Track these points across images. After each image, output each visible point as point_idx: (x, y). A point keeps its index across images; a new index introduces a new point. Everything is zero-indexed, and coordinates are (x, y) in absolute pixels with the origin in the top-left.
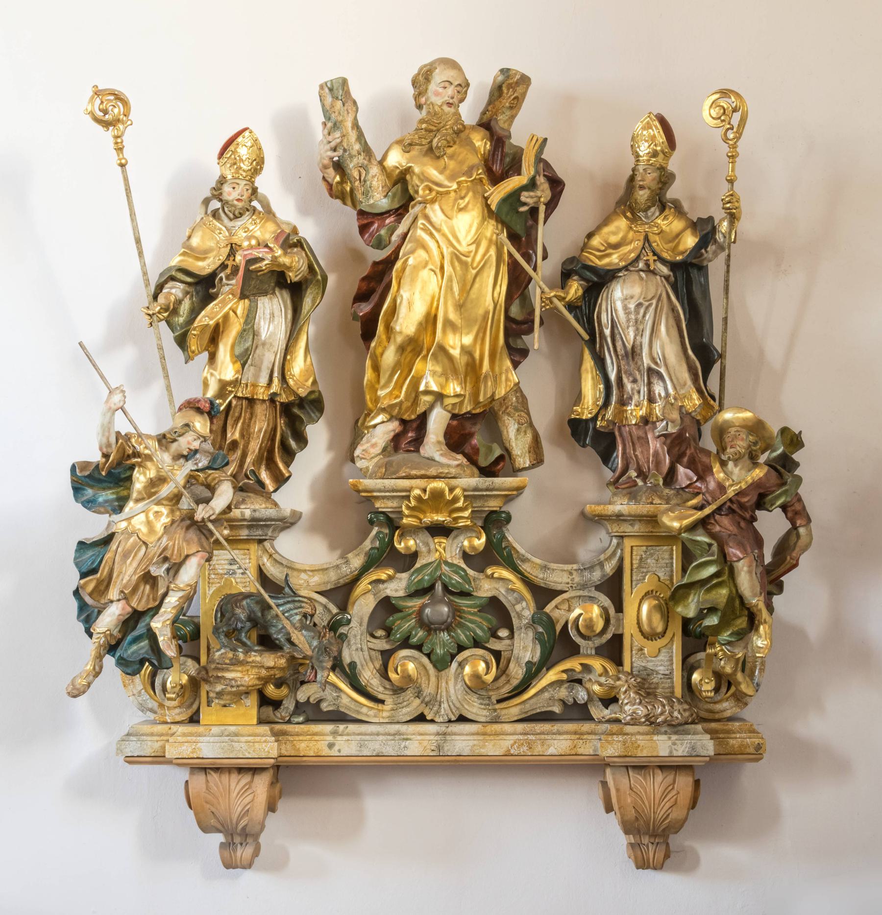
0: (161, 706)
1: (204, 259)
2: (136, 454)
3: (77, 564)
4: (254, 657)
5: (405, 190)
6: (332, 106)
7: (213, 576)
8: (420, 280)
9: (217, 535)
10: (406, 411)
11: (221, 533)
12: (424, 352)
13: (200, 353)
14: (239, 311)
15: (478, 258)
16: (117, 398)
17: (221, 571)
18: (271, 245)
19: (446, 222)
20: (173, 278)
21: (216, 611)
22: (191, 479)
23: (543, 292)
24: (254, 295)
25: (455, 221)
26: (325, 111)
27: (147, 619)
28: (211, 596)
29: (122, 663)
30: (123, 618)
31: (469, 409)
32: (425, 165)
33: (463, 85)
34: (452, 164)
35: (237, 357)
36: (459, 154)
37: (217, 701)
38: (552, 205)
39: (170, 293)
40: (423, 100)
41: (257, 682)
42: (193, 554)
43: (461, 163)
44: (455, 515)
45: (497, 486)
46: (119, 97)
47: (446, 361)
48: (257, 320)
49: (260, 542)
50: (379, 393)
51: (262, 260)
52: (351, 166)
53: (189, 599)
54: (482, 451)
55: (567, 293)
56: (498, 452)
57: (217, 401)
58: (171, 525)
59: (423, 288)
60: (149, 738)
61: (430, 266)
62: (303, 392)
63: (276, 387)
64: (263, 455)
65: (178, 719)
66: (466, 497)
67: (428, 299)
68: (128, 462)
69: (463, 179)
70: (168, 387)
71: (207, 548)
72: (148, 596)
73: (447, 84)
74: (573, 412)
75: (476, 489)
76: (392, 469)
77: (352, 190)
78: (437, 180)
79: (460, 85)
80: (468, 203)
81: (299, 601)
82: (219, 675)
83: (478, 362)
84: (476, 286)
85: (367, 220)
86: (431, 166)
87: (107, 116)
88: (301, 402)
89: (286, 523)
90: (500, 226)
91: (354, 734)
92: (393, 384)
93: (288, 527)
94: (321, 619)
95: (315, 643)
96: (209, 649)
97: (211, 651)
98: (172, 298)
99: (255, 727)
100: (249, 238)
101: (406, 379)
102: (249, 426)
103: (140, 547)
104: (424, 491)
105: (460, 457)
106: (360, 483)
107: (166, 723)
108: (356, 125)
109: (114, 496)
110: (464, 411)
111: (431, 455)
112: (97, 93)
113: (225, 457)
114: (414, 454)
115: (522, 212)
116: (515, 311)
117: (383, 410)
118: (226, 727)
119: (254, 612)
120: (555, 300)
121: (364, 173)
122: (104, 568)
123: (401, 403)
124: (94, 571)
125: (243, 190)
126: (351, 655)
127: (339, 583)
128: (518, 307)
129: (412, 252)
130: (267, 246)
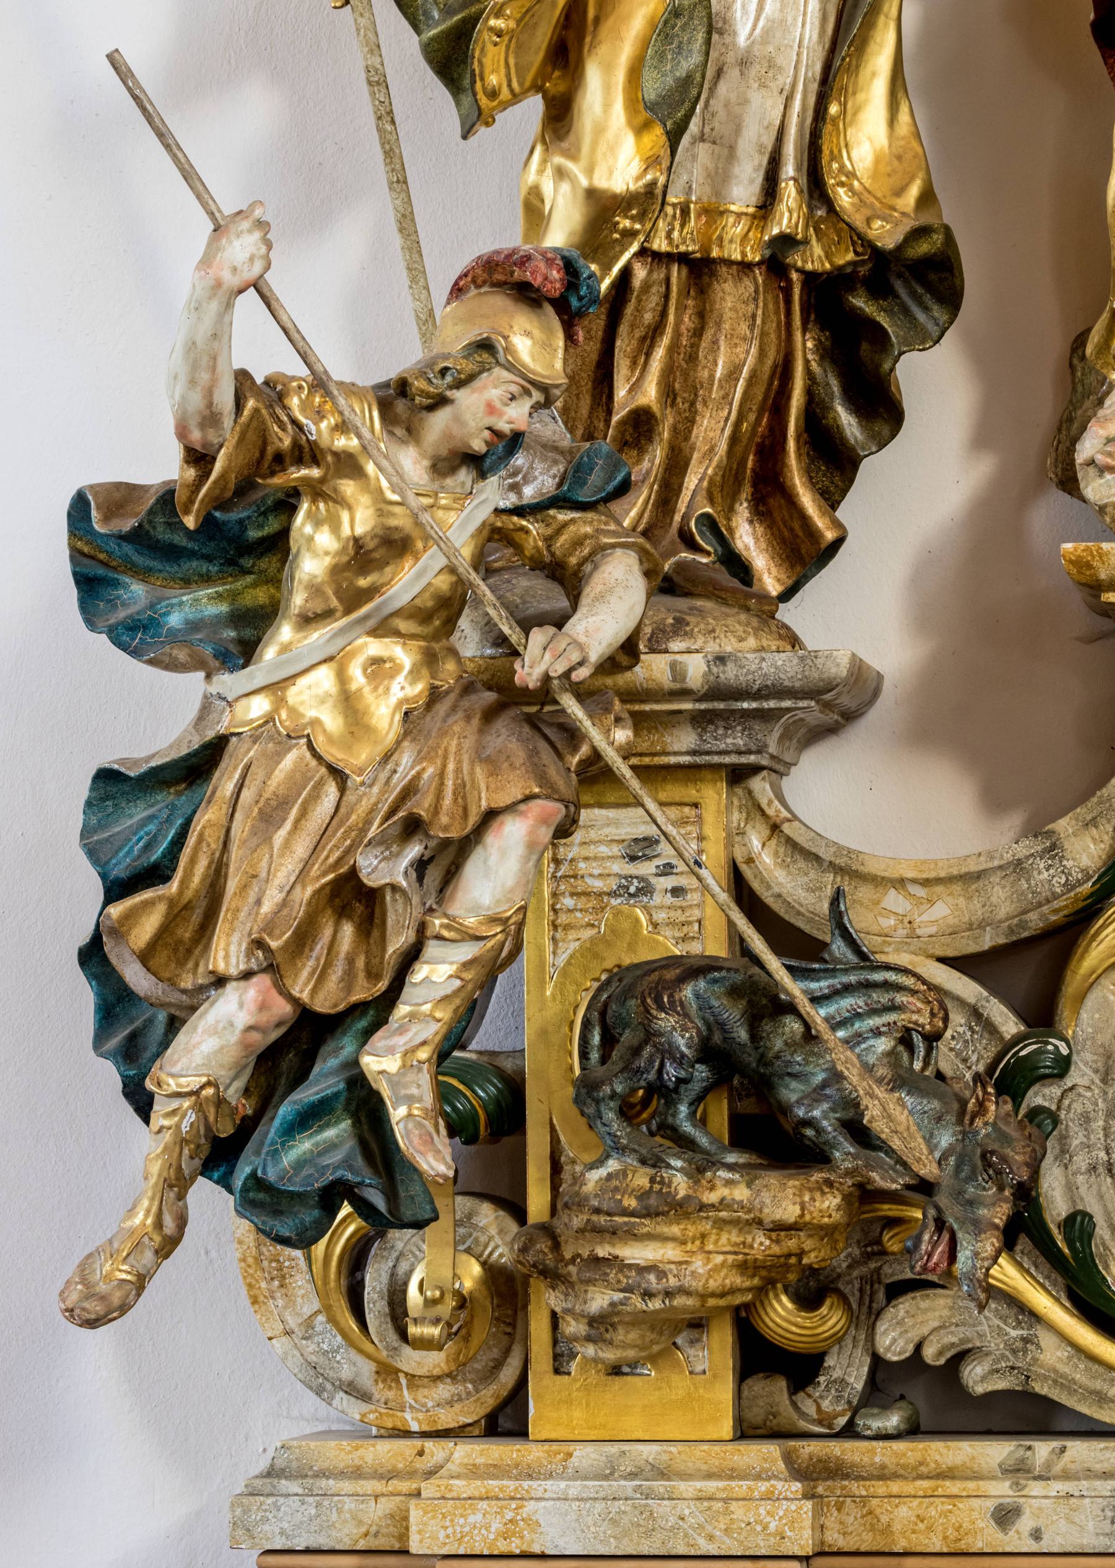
0: (387, 1372)
2: (306, 452)
3: (92, 853)
4: (730, 1188)
7: (568, 902)
9: (595, 735)
11: (611, 739)
13: (516, 98)
16: (241, 248)
17: (598, 885)
21: (586, 1025)
22: (496, 535)
27: (347, 1046)
28: (564, 972)
29: (263, 1200)
30: (261, 1041)
35: (651, 107)
37: (590, 1350)
41: (737, 1280)
42: (510, 808)
49: (738, 775)
53: (489, 972)
60: (347, 1486)
62: (885, 234)
64: (743, 463)
65: (447, 1419)
68: (277, 481)
70: (406, 223)
71: (560, 783)
72: (351, 961)
81: (886, 985)
82: (602, 1252)
88: (882, 270)
89: (833, 706)
91: (1089, 1474)
93: (832, 730)
94: (962, 1055)
95: (945, 1139)
96: (556, 1168)
97: (566, 1175)
99: (730, 1447)
102: (692, 358)
103: (320, 784)
106: (1101, 555)
107: (407, 1434)
109: (223, 608)
113: (615, 466)
118: (626, 1447)
119: (722, 1025)
122: (193, 861)
124: (154, 874)
126: (1070, 1188)
127: (1023, 925)
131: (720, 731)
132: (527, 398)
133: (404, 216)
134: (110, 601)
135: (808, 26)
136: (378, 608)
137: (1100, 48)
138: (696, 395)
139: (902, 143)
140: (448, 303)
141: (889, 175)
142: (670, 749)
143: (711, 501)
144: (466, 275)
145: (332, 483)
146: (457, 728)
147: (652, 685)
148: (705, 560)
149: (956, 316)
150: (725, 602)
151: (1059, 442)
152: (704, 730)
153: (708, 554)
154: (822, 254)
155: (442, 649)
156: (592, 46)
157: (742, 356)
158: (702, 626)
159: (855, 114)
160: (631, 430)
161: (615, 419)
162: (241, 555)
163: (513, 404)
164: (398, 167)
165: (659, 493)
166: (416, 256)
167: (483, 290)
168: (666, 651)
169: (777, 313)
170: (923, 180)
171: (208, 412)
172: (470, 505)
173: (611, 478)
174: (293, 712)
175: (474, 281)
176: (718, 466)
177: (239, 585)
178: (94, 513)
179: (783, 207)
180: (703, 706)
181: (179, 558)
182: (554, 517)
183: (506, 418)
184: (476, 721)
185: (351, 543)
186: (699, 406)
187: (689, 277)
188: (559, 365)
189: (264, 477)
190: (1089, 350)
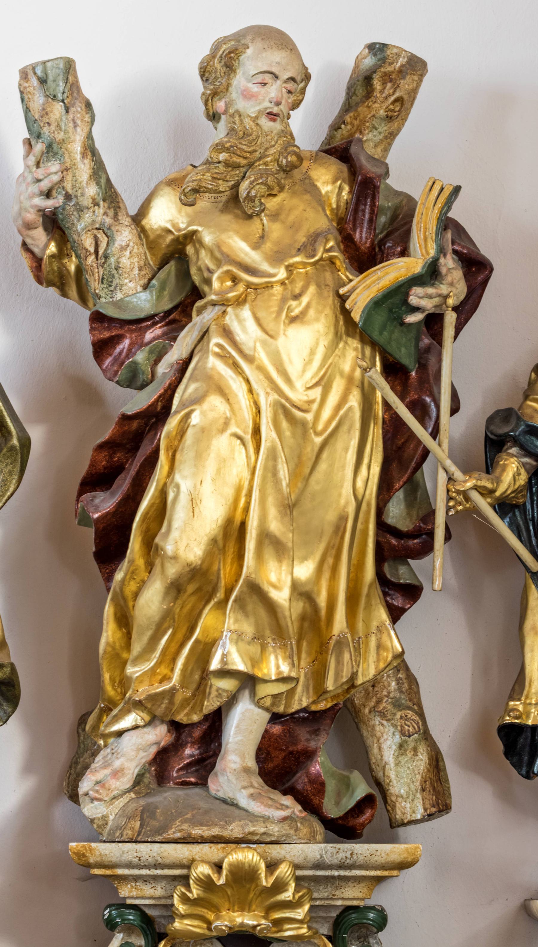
5: (184, 273)
6: (45, 112)
8: (212, 455)
10: (182, 706)
12: (220, 595)
15: (326, 413)
19: (264, 343)
23: (451, 479)
25: (281, 342)
31: (304, 704)
32: (225, 230)
33: (298, 79)
34: (276, 231)
36: (290, 210)
38: (466, 309)
40: (220, 105)
43: (295, 227)
44: (278, 915)
45: (361, 859)
47: (262, 613)
50: (130, 670)
52: (80, 226)
54: (331, 787)
55: (498, 481)
56: (362, 789)
59: (218, 471)
61: (233, 429)
66: (298, 879)
67: (230, 492)
69: (297, 259)
73: (268, 78)
74: (508, 711)
75: (318, 866)
76: (154, 824)
77: (79, 270)
78: (247, 260)
79: (293, 79)
80: (308, 306)
83: (323, 613)
84: (323, 466)
85: (109, 332)
86: (237, 232)
90: (368, 351)
92: (157, 654)
101: (182, 645)
104: (218, 867)
105: (288, 800)
108: (90, 150)
110: (295, 707)
111: (231, 795)
114: (197, 790)
115: (410, 325)
116: (397, 512)
117: (139, 705)
120: (475, 496)
121: (103, 241)
123: (173, 691)
128: (403, 506)
129: (198, 400)
137: (98, 564)
149: (16, 709)
151: (70, 774)
190: (87, 727)
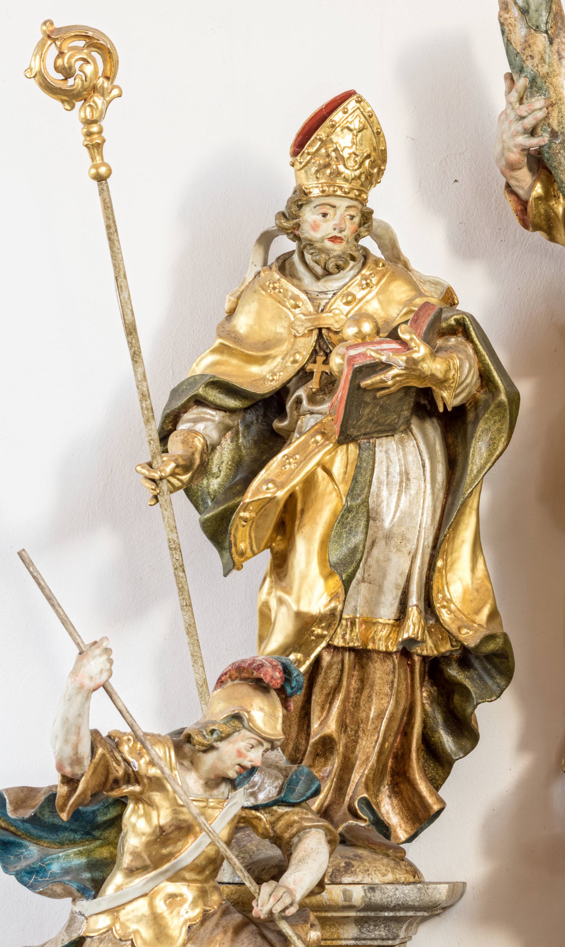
1: (262, 360)
2: (132, 777)
6: (527, 45)
14: (337, 469)
16: (95, 665)
18: (406, 337)
20: (199, 401)
22: (242, 823)
24: (368, 435)
26: (512, 55)
35: (334, 566)
39: (192, 432)
46: (95, 43)
48: (374, 488)
51: (387, 366)
57: (292, 657)
58: (203, 922)
62: (470, 638)
63: (413, 627)
64: (385, 765)
70: (191, 629)
87: (71, 81)
88: (466, 657)
98: (199, 443)
100: (358, 318)
102: (356, 705)
109: (83, 860)
112: (52, 35)
125: (343, 218)
130: (394, 335)
131: (372, 927)
132: (261, 747)
133: (190, 625)
134: (17, 855)
135: (425, 515)
136: (173, 866)
138: (358, 727)
139: (479, 581)
140: (215, 689)
141: (472, 601)
142: (342, 937)
143: (367, 788)
144: (226, 674)
145: (147, 794)
146: (218, 938)
147: (332, 903)
148: (363, 824)
149: (510, 682)
150: (374, 851)
152: (362, 926)
153: (365, 821)
154: (432, 646)
155: (210, 887)
156: (300, 527)
157: (386, 705)
158: (361, 867)
159: (452, 565)
160: (321, 747)
161: (312, 741)
162: (94, 830)
163: (253, 750)
164: (186, 597)
165: (337, 783)
166: (196, 649)
167: (236, 682)
168: (340, 883)
169: (406, 679)
170: (492, 605)
171: (75, 757)
172: (227, 806)
173: (308, 789)
174: (123, 925)
175: (230, 677)
176: (371, 769)
177: (92, 846)
178: (8, 806)
179: (410, 622)
180: (362, 914)
181: (57, 831)
182: (276, 811)
183: (248, 758)
184: (229, 934)
185: (158, 829)
186: (360, 733)
187: (355, 659)
188: (279, 727)
189: (107, 791)
